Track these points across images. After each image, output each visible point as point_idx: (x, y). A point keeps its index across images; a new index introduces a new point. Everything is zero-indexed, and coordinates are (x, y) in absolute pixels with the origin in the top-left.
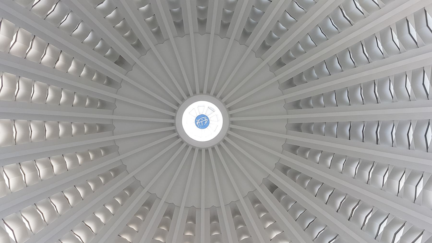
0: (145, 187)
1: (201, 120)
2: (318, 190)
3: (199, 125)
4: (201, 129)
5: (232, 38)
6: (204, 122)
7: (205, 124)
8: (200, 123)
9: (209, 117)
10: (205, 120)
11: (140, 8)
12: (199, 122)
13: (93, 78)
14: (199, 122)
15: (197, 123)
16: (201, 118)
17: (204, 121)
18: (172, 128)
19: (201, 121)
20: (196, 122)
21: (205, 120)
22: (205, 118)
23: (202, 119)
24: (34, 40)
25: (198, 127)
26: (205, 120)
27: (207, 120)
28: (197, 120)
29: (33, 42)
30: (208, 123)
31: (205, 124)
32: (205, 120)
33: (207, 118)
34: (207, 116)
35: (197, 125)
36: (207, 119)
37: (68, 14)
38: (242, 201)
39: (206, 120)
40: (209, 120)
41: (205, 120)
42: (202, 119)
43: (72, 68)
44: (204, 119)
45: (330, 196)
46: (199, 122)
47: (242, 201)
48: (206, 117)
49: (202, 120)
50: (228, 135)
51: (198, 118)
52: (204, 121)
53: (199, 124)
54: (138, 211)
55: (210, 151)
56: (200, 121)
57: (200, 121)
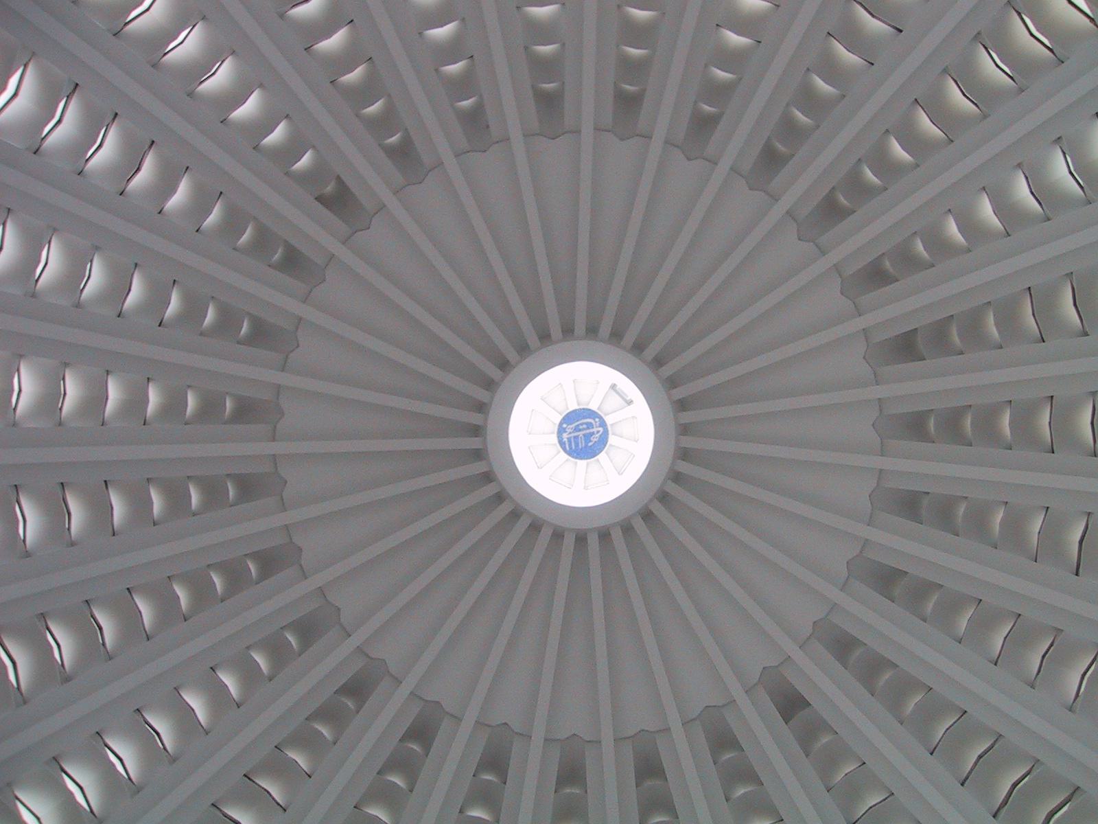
0: (858, 332)
1: (581, 427)
2: (946, 732)
3: (570, 445)
4: (576, 458)
5: (725, 164)
6: (588, 437)
7: (590, 444)
8: (575, 437)
9: (609, 420)
10: (595, 430)
11: (427, 30)
12: (570, 433)
13: (242, 240)
14: (573, 432)
15: (565, 436)
16: (578, 423)
17: (588, 431)
18: (472, 443)
19: (580, 430)
20: (561, 431)
21: (591, 431)
22: (596, 422)
23: (585, 426)
24: (73, 95)
25: (564, 449)
26: (593, 428)
27: (601, 429)
28: (565, 426)
29: (68, 102)
30: (603, 441)
31: (590, 444)
32: (595, 430)
33: (603, 424)
34: (604, 417)
35: (561, 443)
36: (600, 426)
37: (194, 26)
38: (294, 306)
39: (598, 432)
40: (606, 433)
41: (591, 431)
42: (582, 424)
43: (179, 197)
44: (589, 426)
45: (980, 757)
46: (570, 433)
47: (294, 306)
48: (597, 420)
49: (584, 429)
50: (664, 497)
51: (570, 418)
52: (588, 431)
53: (569, 439)
54: (344, 684)
55: (593, 542)
56: (577, 429)
57: (577, 429)
